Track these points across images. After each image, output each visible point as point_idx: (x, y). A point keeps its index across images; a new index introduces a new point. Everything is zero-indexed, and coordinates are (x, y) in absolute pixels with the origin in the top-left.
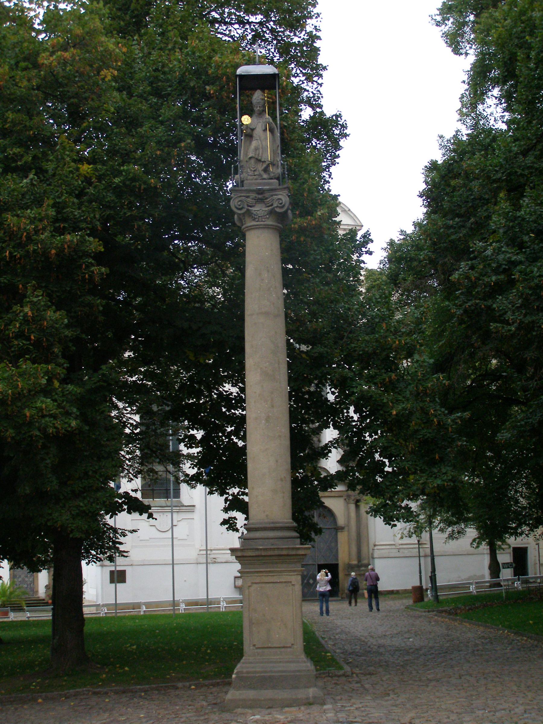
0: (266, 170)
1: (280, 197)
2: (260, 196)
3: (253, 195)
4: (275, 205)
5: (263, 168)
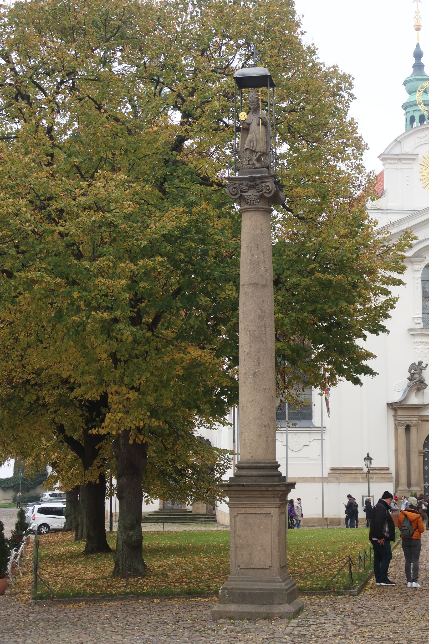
0: (258, 160)
1: (268, 184)
2: (251, 183)
3: (245, 182)
4: (264, 191)
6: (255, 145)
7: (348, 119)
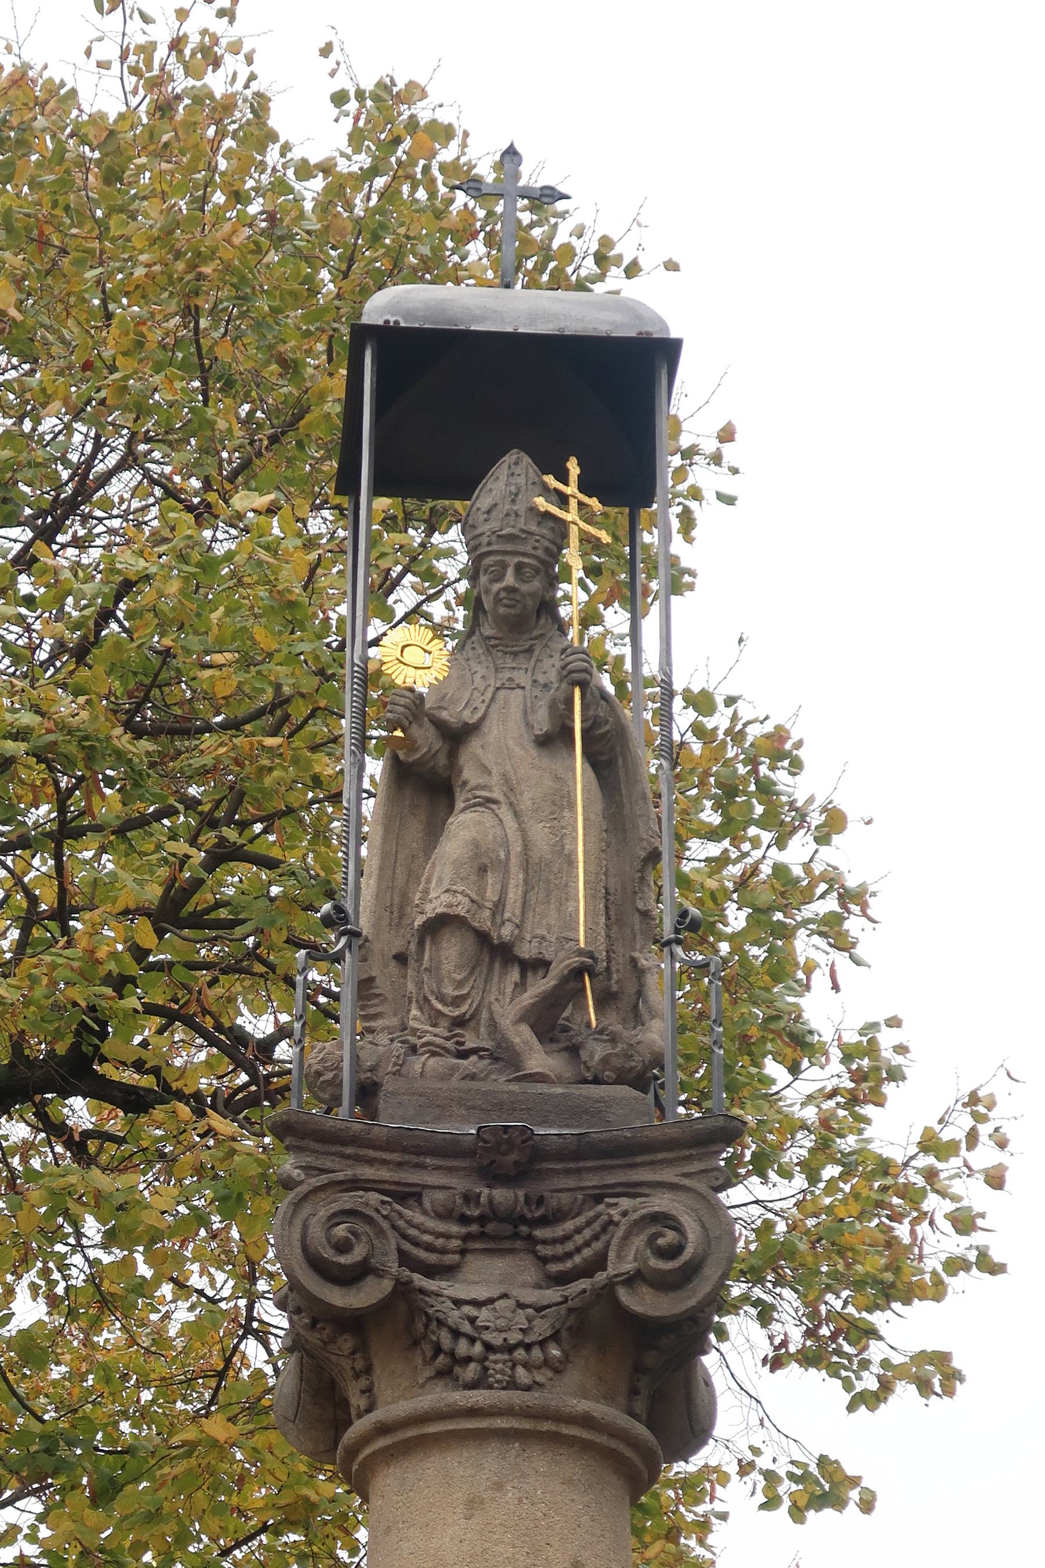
1: (661, 1202)
3: (442, 1184)
5: (527, 998)
6: (514, 895)
7: (312, 130)
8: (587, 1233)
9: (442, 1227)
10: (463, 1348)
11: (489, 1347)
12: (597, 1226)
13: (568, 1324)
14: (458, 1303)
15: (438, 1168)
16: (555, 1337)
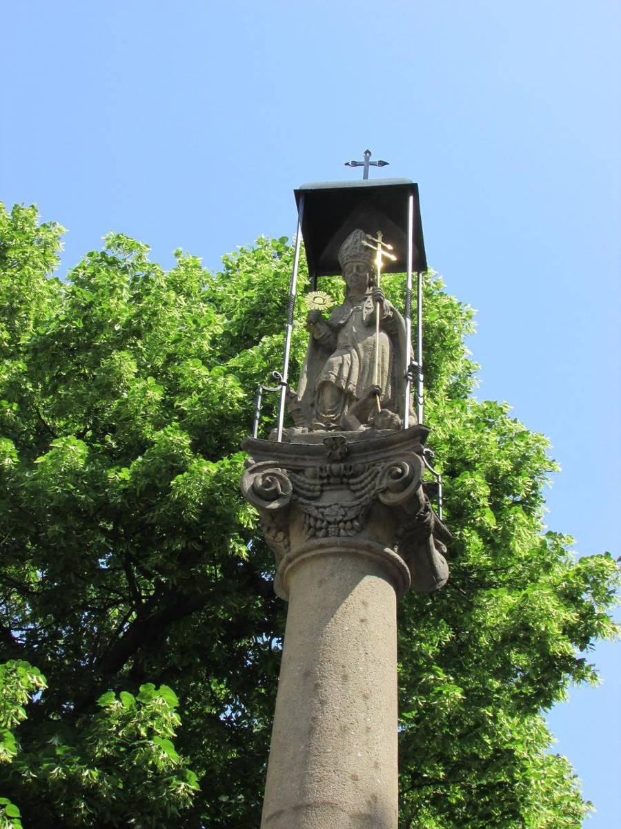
8: (370, 478)
9: (312, 482)
10: (319, 524)
11: (329, 523)
12: (373, 475)
13: (362, 513)
14: (317, 508)
15: (311, 460)
16: (356, 518)
